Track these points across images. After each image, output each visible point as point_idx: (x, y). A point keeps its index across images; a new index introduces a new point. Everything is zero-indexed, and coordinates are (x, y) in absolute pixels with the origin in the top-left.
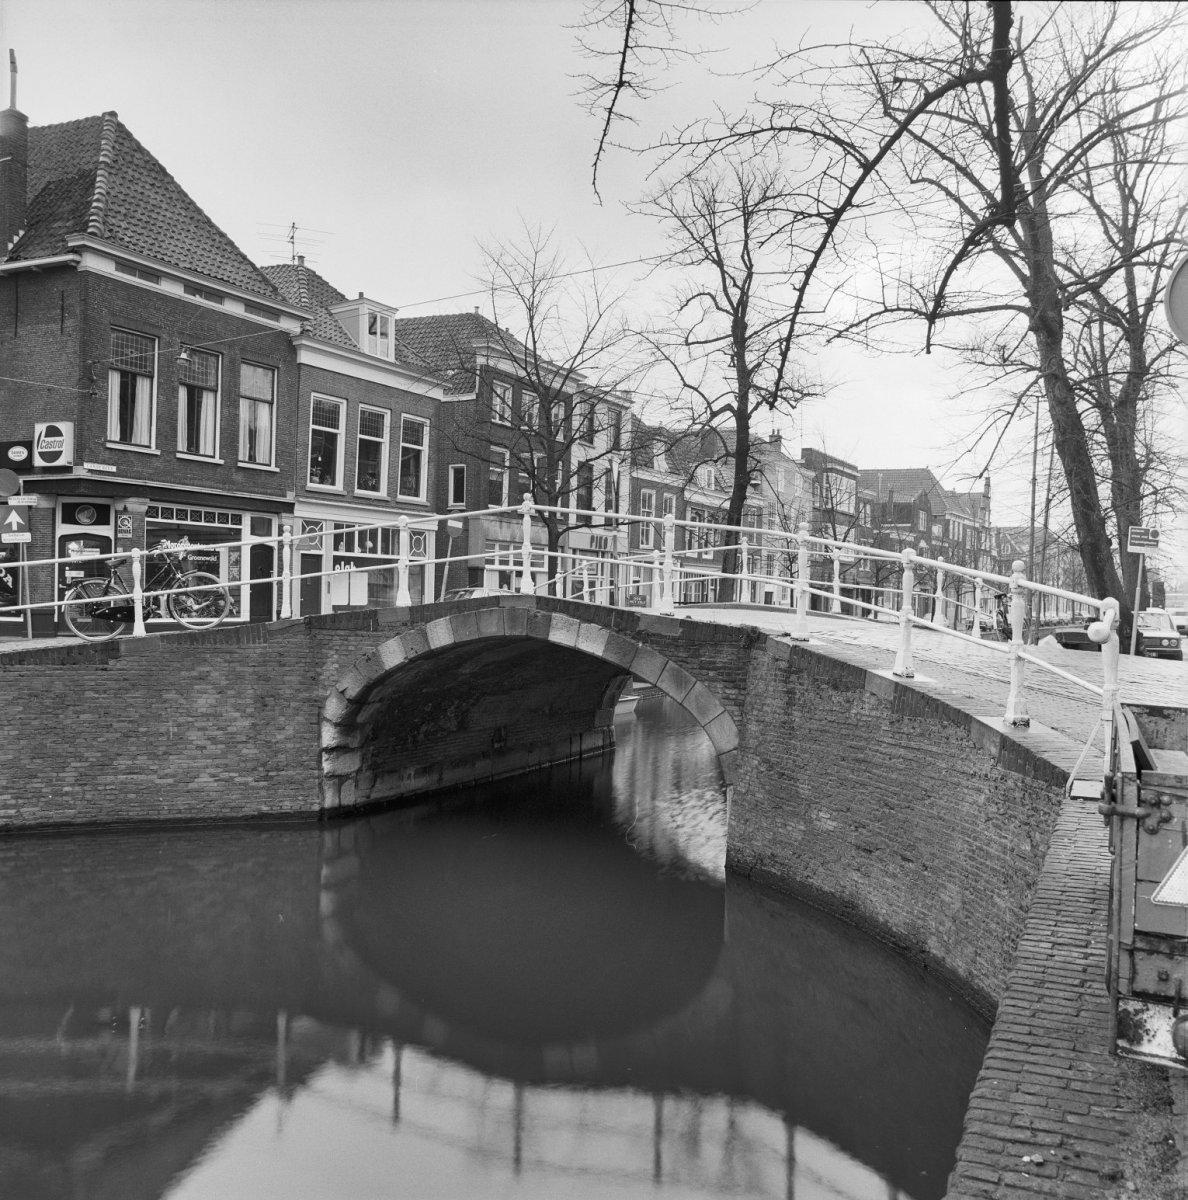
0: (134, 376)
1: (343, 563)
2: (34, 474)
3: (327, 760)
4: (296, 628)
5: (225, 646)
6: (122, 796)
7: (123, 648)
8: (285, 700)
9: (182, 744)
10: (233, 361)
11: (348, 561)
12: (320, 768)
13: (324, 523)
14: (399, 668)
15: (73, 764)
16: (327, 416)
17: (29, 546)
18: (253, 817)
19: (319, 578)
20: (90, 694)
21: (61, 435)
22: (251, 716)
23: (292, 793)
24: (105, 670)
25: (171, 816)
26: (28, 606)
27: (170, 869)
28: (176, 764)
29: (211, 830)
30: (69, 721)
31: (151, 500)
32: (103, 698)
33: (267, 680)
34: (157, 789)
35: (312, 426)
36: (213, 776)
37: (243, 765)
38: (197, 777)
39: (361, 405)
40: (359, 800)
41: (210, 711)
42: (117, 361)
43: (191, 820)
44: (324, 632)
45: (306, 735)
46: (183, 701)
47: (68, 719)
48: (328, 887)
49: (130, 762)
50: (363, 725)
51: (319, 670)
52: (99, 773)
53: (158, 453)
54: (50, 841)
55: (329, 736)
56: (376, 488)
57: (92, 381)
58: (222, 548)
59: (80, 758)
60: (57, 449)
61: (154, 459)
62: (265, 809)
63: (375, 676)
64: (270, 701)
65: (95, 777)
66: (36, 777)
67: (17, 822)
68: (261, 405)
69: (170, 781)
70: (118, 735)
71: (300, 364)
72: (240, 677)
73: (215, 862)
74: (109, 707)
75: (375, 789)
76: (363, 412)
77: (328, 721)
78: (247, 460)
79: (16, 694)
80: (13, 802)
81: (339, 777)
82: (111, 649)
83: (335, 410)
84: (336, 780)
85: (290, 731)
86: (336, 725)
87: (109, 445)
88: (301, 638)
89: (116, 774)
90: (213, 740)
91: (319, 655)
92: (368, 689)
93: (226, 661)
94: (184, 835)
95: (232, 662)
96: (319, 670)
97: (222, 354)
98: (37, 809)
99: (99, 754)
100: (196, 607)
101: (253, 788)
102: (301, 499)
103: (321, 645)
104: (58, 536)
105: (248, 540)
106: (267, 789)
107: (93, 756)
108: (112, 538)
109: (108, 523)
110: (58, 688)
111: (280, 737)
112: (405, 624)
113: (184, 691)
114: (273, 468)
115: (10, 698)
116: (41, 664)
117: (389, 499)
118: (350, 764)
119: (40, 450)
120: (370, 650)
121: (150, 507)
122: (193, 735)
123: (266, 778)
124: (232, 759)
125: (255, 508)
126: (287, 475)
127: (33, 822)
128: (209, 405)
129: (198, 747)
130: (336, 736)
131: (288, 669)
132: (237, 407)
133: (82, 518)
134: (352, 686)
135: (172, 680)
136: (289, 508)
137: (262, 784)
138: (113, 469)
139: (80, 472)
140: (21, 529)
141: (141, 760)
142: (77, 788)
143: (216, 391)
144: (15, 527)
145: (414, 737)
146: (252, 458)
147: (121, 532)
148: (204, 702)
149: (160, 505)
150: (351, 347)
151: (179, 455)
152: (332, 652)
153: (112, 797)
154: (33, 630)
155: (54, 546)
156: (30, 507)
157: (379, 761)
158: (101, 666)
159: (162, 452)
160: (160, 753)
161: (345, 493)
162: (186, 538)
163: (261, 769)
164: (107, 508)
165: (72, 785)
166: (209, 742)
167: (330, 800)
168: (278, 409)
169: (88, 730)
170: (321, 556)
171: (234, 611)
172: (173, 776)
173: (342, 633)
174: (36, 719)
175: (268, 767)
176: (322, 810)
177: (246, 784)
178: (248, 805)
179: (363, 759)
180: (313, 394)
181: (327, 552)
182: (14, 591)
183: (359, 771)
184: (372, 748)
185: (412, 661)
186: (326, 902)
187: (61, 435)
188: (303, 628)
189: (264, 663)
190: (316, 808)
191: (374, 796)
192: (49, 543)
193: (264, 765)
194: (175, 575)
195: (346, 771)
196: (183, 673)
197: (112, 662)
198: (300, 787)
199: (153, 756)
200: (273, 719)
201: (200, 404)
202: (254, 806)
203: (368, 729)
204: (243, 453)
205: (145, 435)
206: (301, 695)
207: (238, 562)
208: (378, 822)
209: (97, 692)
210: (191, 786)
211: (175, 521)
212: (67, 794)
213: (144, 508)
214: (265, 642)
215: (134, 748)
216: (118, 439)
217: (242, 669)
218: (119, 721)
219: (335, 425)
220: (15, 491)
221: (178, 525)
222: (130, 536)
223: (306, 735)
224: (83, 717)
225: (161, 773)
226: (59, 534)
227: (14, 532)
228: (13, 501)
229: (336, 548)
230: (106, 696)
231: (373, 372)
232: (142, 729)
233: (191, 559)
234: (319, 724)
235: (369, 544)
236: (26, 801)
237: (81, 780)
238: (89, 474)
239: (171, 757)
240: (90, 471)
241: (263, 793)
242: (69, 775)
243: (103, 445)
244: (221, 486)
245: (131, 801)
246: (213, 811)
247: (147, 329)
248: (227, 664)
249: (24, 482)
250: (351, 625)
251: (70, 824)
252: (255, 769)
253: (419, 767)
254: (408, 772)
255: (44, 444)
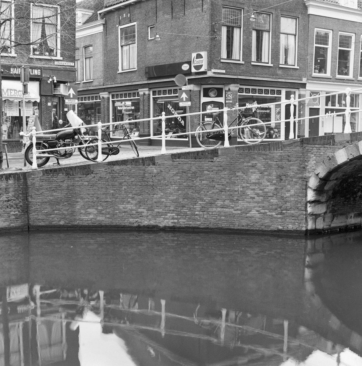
0: (233, 27)
1: (330, 112)
2: (192, 75)
3: (310, 207)
4: (296, 144)
5: (263, 152)
6: (219, 217)
7: (219, 152)
8: (291, 177)
9: (244, 196)
10: (277, 16)
11: (332, 111)
12: (306, 211)
13: (321, 92)
14: (345, 164)
15: (199, 202)
16: (323, 39)
17: (190, 107)
18: (275, 231)
19: (318, 118)
20: (206, 172)
21: (202, 57)
22: (275, 184)
23: (293, 221)
24: (212, 162)
25: (239, 228)
26: (190, 133)
27: (239, 251)
28: (242, 204)
29: (256, 235)
30: (198, 184)
31: (240, 85)
32: (212, 174)
33: (282, 168)
34: (234, 216)
35: (315, 45)
36: (257, 211)
37: (271, 207)
38: (251, 211)
39: (340, 32)
40: (325, 227)
41: (257, 181)
42: (225, 22)
43: (248, 230)
44: (309, 146)
45: (300, 195)
46: (245, 176)
47: (197, 183)
48: (309, 267)
49: (222, 203)
50: (328, 191)
51: (306, 164)
52: (209, 207)
53: (243, 63)
54: (191, 234)
55: (311, 195)
56: (347, 74)
57: (214, 32)
58: (272, 105)
59: (202, 200)
60: (201, 64)
61: (242, 66)
62: (280, 227)
63: (333, 167)
64: (283, 178)
65: (208, 209)
66: (185, 207)
67: (178, 225)
68: (290, 36)
69: (239, 212)
70: (218, 191)
71: (309, 14)
72: (270, 166)
73: (258, 250)
74: (214, 178)
75: (333, 222)
76: (341, 36)
77: (311, 188)
78: (284, 63)
79: (177, 171)
80: (176, 217)
81: (315, 215)
82: (215, 153)
83: (326, 36)
84: (314, 217)
85: (292, 192)
86: (314, 190)
87: (222, 61)
88: (298, 148)
89: (217, 208)
90: (258, 195)
91: (307, 157)
92: (330, 174)
93: (264, 159)
94: (245, 236)
95: (267, 159)
96: (306, 164)
97: (272, 13)
98: (186, 220)
99: (210, 199)
100: (260, 134)
101: (275, 218)
102: (309, 81)
103: (308, 151)
104: (202, 103)
105: (284, 102)
106: (282, 218)
107: (207, 199)
108: (224, 103)
109: (222, 96)
110: (194, 169)
111: (288, 195)
112: (348, 142)
113: (245, 172)
114: (296, 67)
115: (175, 173)
116: (187, 159)
117: (354, 79)
118: (321, 209)
119: (194, 65)
120: (330, 155)
121: (239, 88)
122: (249, 192)
123: (281, 213)
124: (266, 204)
125: (287, 87)
126: (303, 69)
127: (184, 226)
128: (266, 37)
129: (251, 198)
130: (314, 195)
131: (292, 163)
132: (279, 38)
133: (211, 94)
134: (322, 172)
135: (240, 167)
136: (304, 85)
137: (279, 216)
138: (224, 71)
139: (210, 74)
140: (187, 100)
141: (227, 202)
142: (201, 213)
143: (269, 32)
144: (184, 100)
145: (354, 198)
146: (286, 62)
147: (228, 100)
148: (254, 177)
149: (244, 87)
150: (335, 4)
151: (252, 63)
152: (312, 155)
153: (215, 218)
154: (192, 144)
155: (200, 107)
156: (190, 90)
157: (336, 209)
158: (211, 160)
159: (245, 62)
160: (235, 200)
161: (331, 77)
162: (256, 102)
163: (279, 209)
164: (221, 89)
165: (199, 211)
166: (256, 196)
167: (310, 226)
168: (298, 38)
169: (205, 188)
170: (319, 109)
171: (278, 136)
172: (241, 210)
173: (316, 146)
174: (185, 182)
175: (282, 209)
176: (307, 230)
177: (272, 216)
178: (273, 225)
179: (327, 208)
180: (316, 29)
181: (322, 107)
182: (185, 127)
183: (325, 213)
184: (332, 202)
185: (351, 160)
186: (308, 273)
187: (202, 57)
188: (299, 143)
189: (281, 160)
190: (304, 229)
191: (333, 225)
192: (198, 106)
193: (280, 207)
194: (242, 119)
195: (319, 212)
196: (245, 164)
197: (215, 158)
198: (296, 218)
199: (232, 201)
200: (285, 186)
201: (262, 37)
202: (276, 226)
203: (330, 193)
204: (282, 61)
205: (237, 54)
206: (298, 176)
207: (279, 113)
208: (335, 238)
209: (209, 171)
210: (248, 215)
211: (251, 94)
212: (197, 215)
213: (237, 89)
214: (282, 150)
215: (224, 197)
216: (226, 57)
217: (271, 163)
218: (218, 185)
219: (326, 43)
220: (184, 84)
221: (253, 96)
222: (231, 102)
223: (300, 195)
224: (203, 182)
225: (236, 208)
226: (202, 101)
227: (185, 101)
228: (184, 88)
229: (327, 105)
230: (212, 173)
231: (339, 13)
232: (227, 189)
233: (258, 111)
234: (306, 189)
235: (343, 102)
236: (181, 217)
237: (203, 209)
238: (214, 74)
239: (239, 201)
240: (214, 73)
241: (280, 220)
242: (198, 207)
243: (220, 60)
244: (272, 77)
245: (223, 220)
246: (257, 227)
247: (238, 5)
248: (264, 160)
249: (188, 79)
250: (322, 142)
251: (198, 228)
252: (276, 209)
253: (356, 212)
254: (350, 215)
255: (196, 62)
